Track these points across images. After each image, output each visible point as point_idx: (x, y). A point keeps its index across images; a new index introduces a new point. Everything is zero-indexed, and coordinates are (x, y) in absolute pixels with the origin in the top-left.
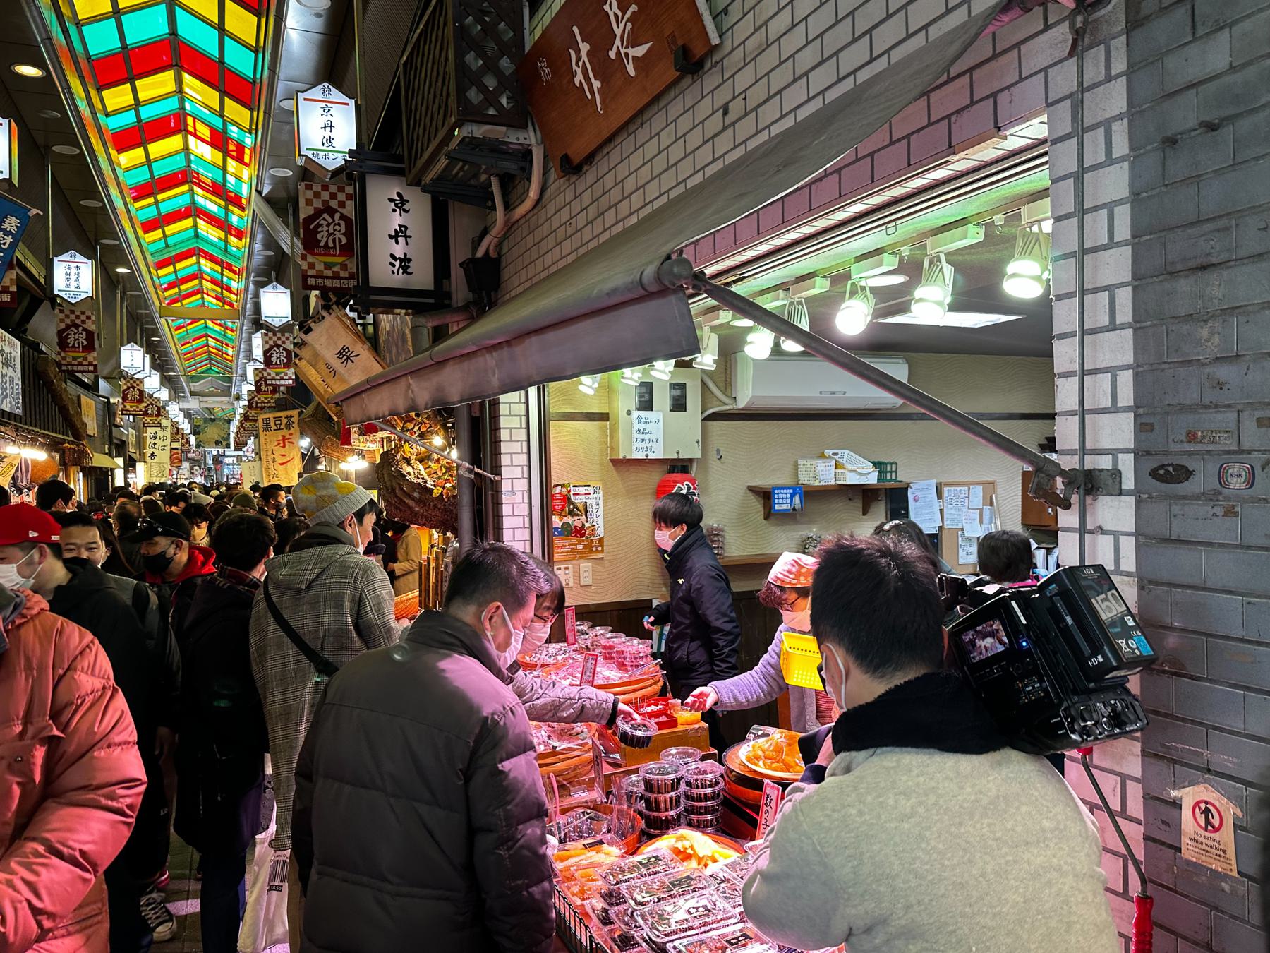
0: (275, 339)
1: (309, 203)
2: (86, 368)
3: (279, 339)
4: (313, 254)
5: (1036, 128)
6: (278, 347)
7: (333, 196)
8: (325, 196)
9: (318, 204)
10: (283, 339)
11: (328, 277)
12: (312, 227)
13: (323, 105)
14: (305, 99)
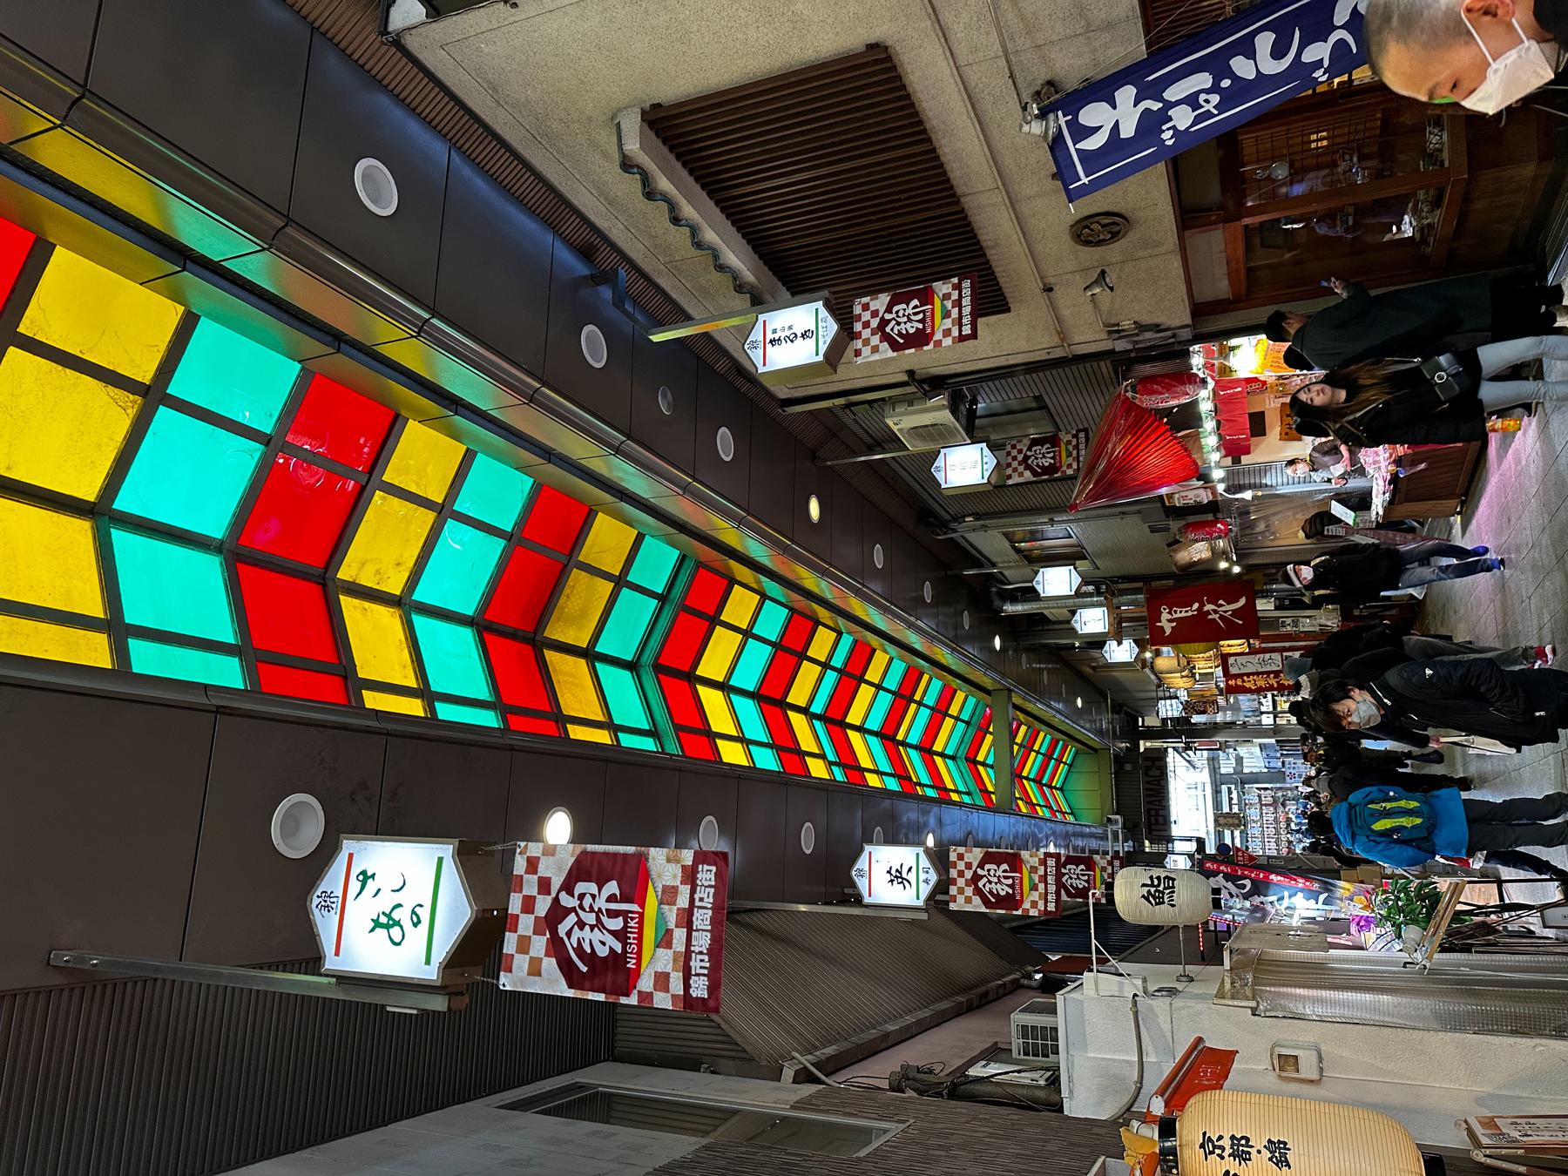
0: (961, 882)
1: (875, 350)
3: (1015, 458)
6: (1026, 458)
7: (1015, 458)
11: (1078, 453)
12: (902, 341)
13: (769, 346)
14: (764, 365)
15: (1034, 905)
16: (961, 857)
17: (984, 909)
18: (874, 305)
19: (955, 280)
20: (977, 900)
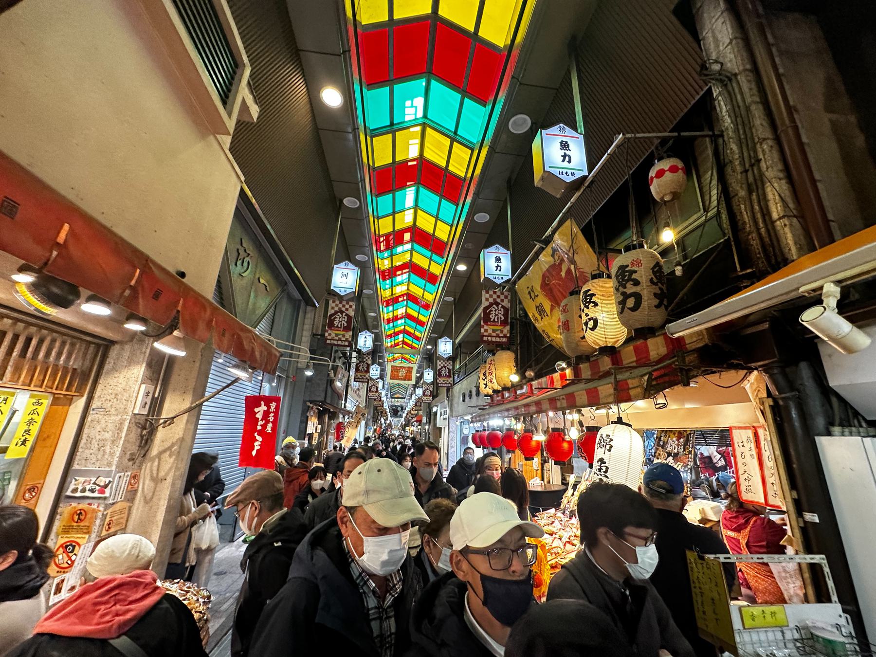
0: (340, 306)
1: (487, 300)
2: (343, 343)
4: (487, 325)
5: (225, 606)
8: (495, 296)
9: (491, 300)
10: (347, 306)
15: (486, 331)
16: (351, 307)
17: (329, 314)
18: (506, 301)
19: (508, 335)
20: (333, 311)
